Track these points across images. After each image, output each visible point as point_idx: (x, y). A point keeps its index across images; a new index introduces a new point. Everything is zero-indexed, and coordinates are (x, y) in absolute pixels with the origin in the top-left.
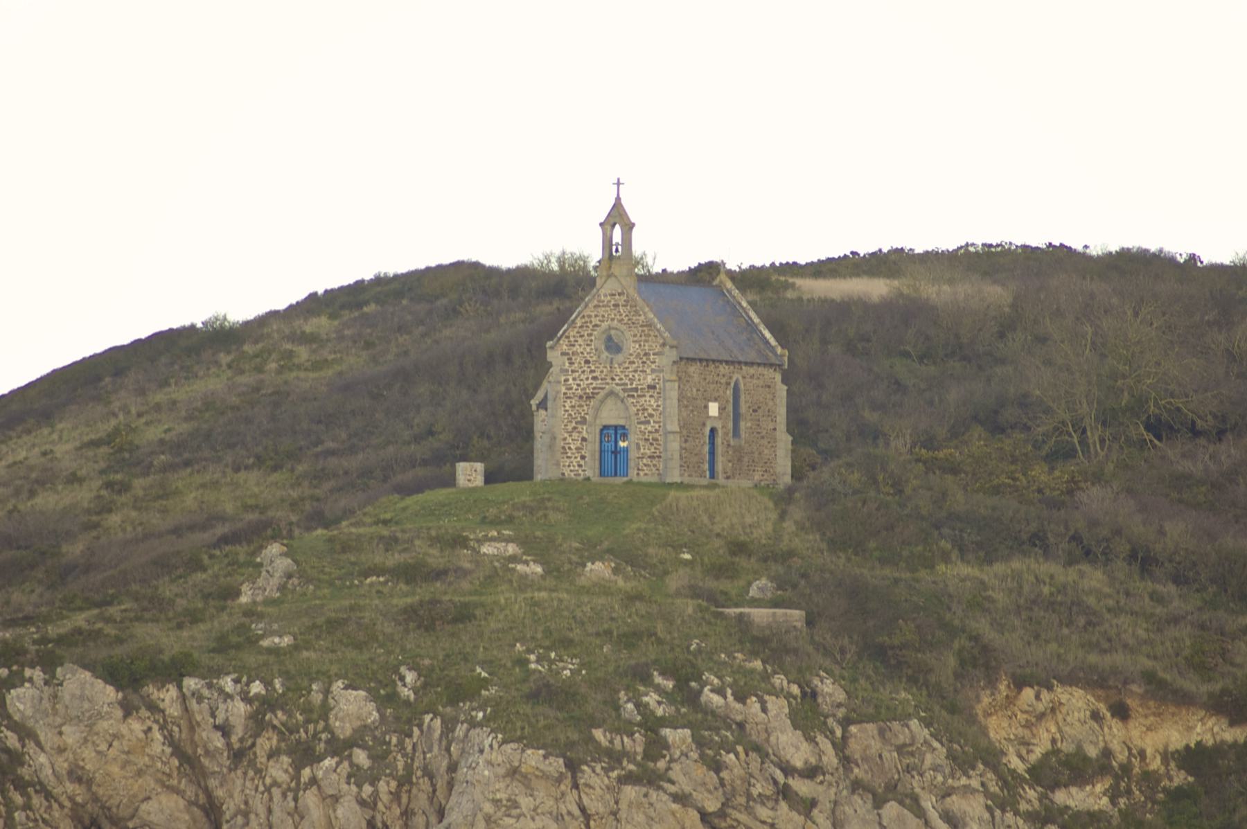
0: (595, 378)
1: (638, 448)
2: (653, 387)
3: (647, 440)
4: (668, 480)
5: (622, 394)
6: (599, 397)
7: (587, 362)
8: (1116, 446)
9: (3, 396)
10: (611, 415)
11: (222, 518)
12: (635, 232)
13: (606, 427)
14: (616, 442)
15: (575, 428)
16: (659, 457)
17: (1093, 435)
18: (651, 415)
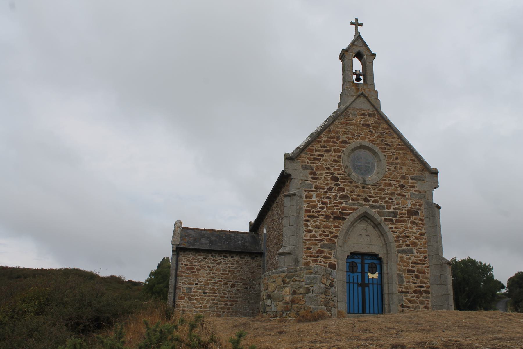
0: (344, 197)
1: (401, 281)
2: (416, 213)
3: (410, 271)
4: (391, 305)
5: (378, 218)
6: (351, 218)
7: (335, 179)
8: (300, 303)
9: (1, 267)
10: (364, 240)
11: (217, 264)
12: (376, 63)
13: (354, 254)
14: (363, 273)
15: (320, 252)
16: (427, 292)
17: (423, 297)
18: (414, 244)
